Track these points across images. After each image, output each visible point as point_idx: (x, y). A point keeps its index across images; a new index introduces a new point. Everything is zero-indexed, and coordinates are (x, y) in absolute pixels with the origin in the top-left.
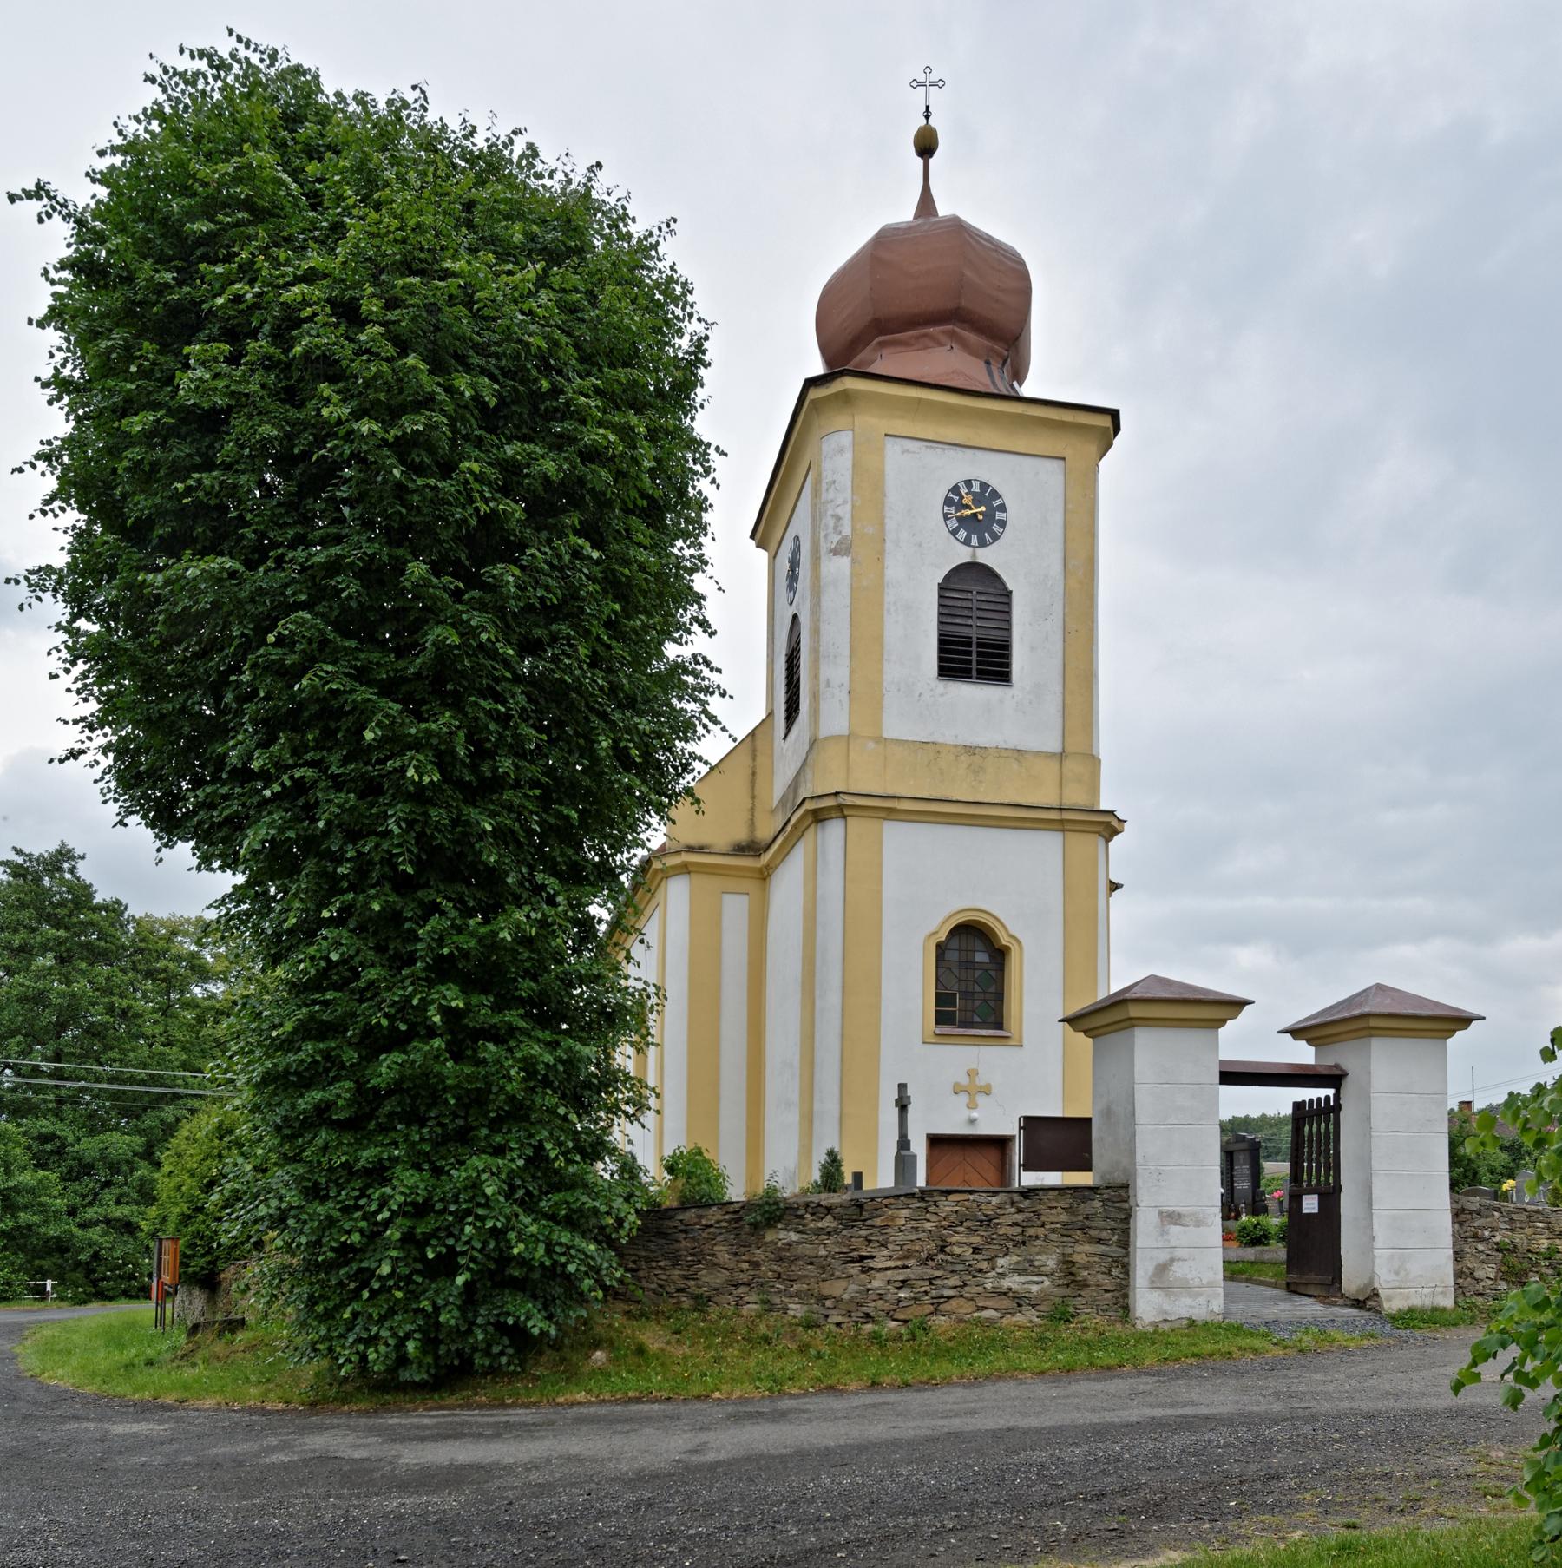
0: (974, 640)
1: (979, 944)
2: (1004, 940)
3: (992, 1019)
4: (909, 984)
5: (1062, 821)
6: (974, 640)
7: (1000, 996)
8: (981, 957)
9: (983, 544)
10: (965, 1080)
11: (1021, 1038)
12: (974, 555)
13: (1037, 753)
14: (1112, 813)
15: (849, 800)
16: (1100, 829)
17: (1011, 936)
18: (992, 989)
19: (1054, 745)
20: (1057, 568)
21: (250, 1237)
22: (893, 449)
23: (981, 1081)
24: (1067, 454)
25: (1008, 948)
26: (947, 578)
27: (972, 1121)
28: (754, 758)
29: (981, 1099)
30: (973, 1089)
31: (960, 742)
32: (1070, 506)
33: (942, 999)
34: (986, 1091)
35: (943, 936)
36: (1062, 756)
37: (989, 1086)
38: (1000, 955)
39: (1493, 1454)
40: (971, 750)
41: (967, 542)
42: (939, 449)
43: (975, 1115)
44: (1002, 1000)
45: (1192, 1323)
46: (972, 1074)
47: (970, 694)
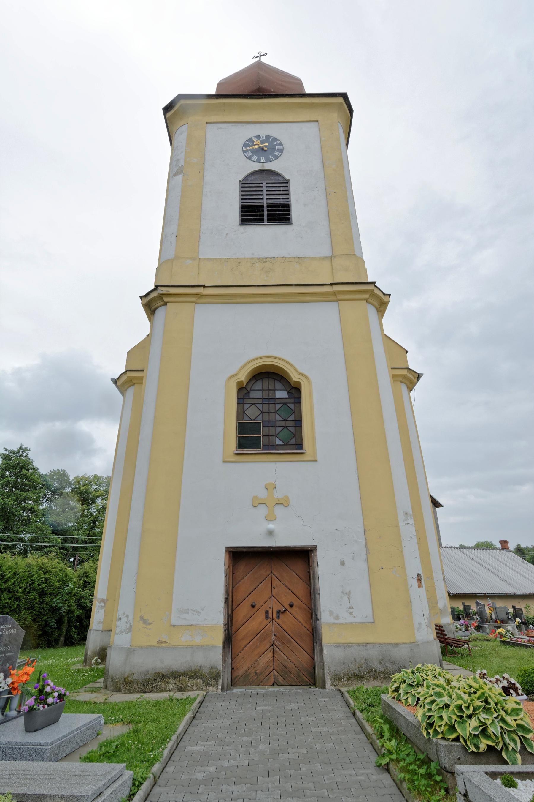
0: (265, 205)
1: (278, 385)
2: (294, 377)
3: (293, 441)
4: (215, 415)
5: (334, 293)
6: (265, 205)
7: (298, 423)
8: (281, 394)
9: (268, 161)
10: (263, 494)
11: (315, 453)
12: (263, 166)
13: (314, 258)
14: (374, 283)
15: (165, 290)
16: (366, 296)
17: (301, 374)
18: (292, 418)
19: (327, 253)
20: (317, 165)
21: (51, 774)
22: (212, 130)
23: (278, 494)
24: (319, 118)
25: (299, 383)
26: (246, 178)
27: (270, 533)
28: (444, 578)
29: (279, 511)
30: (273, 503)
31: (256, 256)
32: (323, 139)
33: (242, 427)
34: (284, 503)
35: (243, 377)
36: (331, 259)
37: (287, 498)
38: (295, 391)
39: (201, 683)
40: (263, 260)
41: (258, 161)
42: (240, 126)
43: (271, 526)
44: (301, 426)
45: (225, 603)
46: (270, 487)
47: (264, 234)
